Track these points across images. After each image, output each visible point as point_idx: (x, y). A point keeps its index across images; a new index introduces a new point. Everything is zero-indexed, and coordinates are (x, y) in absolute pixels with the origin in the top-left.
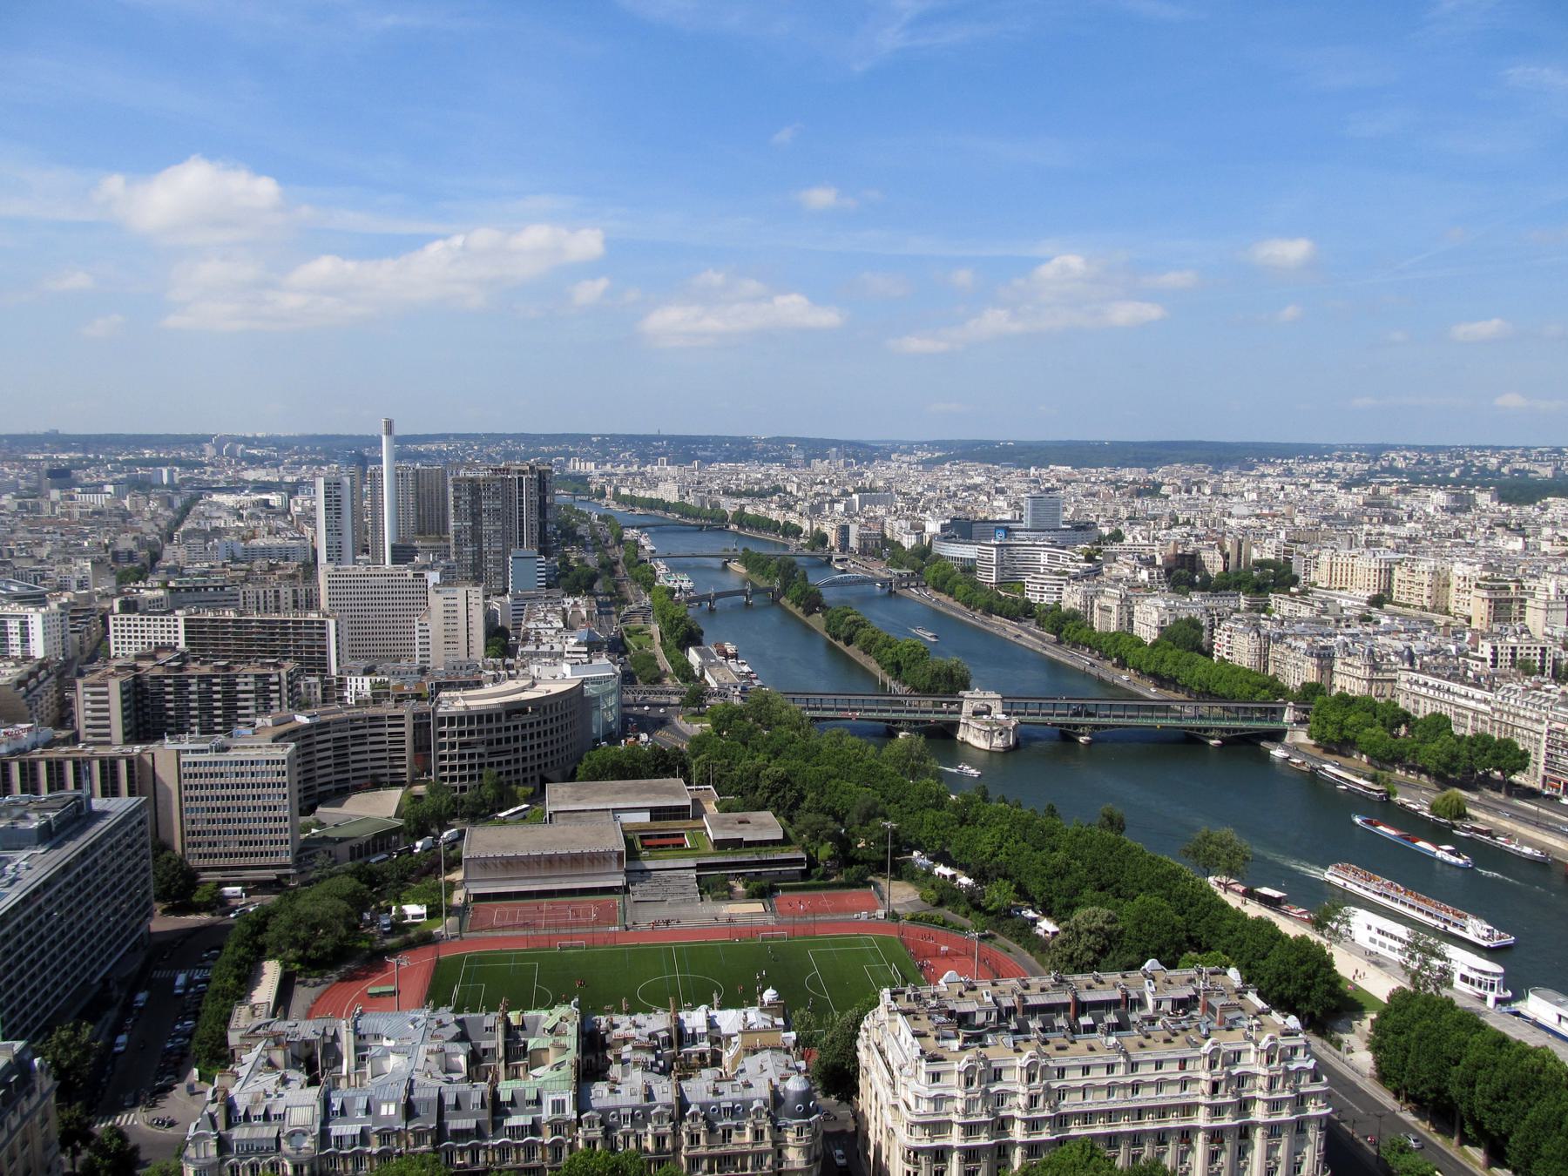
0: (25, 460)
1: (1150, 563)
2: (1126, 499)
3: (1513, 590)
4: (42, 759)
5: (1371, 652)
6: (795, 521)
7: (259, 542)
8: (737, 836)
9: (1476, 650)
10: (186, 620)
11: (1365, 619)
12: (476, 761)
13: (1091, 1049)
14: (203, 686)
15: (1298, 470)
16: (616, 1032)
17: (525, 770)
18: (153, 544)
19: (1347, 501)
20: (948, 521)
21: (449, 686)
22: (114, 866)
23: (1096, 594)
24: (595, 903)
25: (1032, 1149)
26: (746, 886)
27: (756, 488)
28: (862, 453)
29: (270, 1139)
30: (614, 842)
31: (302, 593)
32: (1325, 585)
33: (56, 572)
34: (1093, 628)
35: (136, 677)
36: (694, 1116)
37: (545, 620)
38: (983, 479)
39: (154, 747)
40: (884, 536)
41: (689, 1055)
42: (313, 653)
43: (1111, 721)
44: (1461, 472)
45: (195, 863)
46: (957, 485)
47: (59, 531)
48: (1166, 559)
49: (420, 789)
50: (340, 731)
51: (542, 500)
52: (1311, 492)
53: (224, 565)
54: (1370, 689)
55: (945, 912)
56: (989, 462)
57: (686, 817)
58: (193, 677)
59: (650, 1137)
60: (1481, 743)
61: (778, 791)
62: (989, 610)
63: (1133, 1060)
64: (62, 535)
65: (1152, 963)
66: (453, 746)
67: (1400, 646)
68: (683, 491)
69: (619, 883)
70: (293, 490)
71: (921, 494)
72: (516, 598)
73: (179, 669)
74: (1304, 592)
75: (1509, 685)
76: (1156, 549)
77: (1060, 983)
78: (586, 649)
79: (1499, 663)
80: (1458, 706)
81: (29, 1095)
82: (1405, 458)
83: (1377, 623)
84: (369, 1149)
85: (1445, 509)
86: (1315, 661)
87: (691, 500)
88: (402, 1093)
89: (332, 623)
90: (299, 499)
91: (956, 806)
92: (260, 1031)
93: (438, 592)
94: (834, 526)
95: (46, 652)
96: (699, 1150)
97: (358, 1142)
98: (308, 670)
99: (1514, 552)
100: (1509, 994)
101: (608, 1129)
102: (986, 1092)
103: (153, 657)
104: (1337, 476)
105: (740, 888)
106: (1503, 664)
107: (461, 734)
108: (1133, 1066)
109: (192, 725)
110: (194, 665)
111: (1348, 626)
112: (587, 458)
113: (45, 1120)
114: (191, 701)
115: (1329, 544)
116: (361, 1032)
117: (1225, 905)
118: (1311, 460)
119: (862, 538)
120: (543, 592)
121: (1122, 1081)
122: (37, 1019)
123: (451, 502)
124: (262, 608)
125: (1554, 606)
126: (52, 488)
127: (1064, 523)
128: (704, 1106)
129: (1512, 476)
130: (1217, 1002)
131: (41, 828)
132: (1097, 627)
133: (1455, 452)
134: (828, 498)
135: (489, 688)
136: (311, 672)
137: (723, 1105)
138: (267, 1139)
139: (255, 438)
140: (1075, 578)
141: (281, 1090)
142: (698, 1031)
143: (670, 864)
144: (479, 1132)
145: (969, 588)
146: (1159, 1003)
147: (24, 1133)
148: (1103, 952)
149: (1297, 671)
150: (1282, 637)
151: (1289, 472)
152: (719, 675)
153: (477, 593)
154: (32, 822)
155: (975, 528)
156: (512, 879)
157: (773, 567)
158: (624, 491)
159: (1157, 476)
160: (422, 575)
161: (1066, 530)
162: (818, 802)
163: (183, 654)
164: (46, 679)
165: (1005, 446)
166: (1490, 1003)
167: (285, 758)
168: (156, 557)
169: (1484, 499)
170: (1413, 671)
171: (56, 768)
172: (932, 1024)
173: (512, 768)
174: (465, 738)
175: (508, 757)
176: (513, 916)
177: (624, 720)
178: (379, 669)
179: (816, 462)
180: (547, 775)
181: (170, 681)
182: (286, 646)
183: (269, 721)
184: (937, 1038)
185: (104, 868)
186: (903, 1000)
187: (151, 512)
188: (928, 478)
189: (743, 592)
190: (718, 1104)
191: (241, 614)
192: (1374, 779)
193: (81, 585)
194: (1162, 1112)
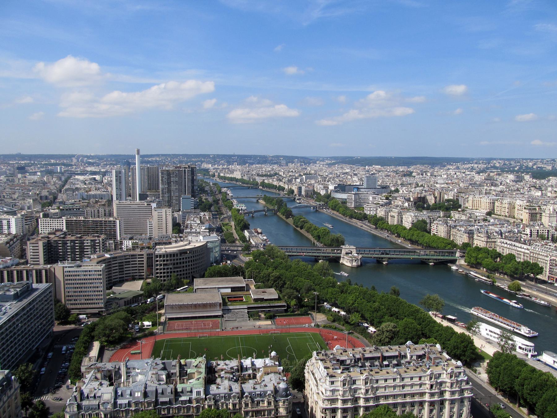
0: (9, 164)
1: (408, 200)
2: (400, 177)
3: (537, 210)
4: (15, 270)
5: (487, 232)
6: (282, 185)
7: (92, 193)
8: (262, 297)
9: (524, 231)
10: (66, 220)
11: (485, 220)
12: (169, 270)
13: (388, 373)
14: (72, 244)
15: (461, 167)
16: (219, 367)
17: (186, 274)
18: (54, 193)
19: (478, 178)
20: (337, 185)
21: (159, 244)
22: (41, 308)
23: (389, 211)
24: (211, 321)
25: (367, 408)
26: (265, 315)
27: (269, 173)
28: (306, 161)
29: (96, 405)
30: (218, 299)
31: (107, 211)
32: (471, 208)
33: (20, 203)
34: (388, 223)
35: (48, 241)
36: (247, 397)
37: (194, 221)
38: (349, 170)
39: (55, 265)
40: (314, 190)
41: (245, 375)
42: (111, 232)
43: (395, 256)
44: (519, 168)
45: (69, 307)
46: (340, 173)
47: (21, 189)
48: (414, 199)
49: (149, 281)
50: (121, 260)
51: (193, 178)
52: (466, 175)
53: (80, 201)
54: (487, 245)
56: (351, 164)
57: (244, 290)
58: (68, 241)
59: (231, 404)
60: (526, 264)
61: (276, 281)
62: (351, 217)
63: (403, 377)
64: (22, 190)
65: (409, 342)
66: (161, 265)
67: (497, 230)
68: (243, 174)
69: (220, 314)
71: (327, 176)
72: (183, 213)
73: (64, 238)
74: (463, 211)
75: (536, 244)
76: (411, 195)
77: (377, 349)
78: (208, 231)
79: (533, 236)
80: (518, 251)
81: (10, 389)
82: (499, 163)
83: (489, 221)
84: (131, 409)
85: (513, 181)
86: (467, 235)
87: (245, 178)
88: (143, 389)
89: (118, 221)
90: (106, 177)
91: (340, 287)
92: (93, 367)
93: (155, 210)
94: (296, 187)
95: (16, 232)
96: (248, 409)
97: (127, 406)
98: (109, 238)
99: (538, 196)
100: (536, 353)
101: (216, 401)
102: (350, 388)
103: (54, 234)
104: (475, 169)
105: (263, 316)
106: (534, 236)
107: (164, 261)
108: (403, 379)
109: (68, 258)
110: (69, 236)
111: (479, 223)
112: (208, 163)
113: (16, 398)
114: (68, 249)
115: (472, 193)
116: (128, 367)
117: (435, 322)
118: (466, 164)
119: (306, 191)
120: (193, 211)
121: (399, 384)
122: (13, 362)
123: (160, 179)
124: (93, 216)
125: (552, 215)
126: (19, 173)
127: (378, 186)
128: (250, 393)
129: (537, 169)
130: (432, 356)
131: (14, 294)
132: (390, 223)
133: (517, 161)
134: (294, 177)
135: (174, 245)
136: (111, 239)
137: (257, 393)
138: (95, 405)
139: (91, 156)
140: (382, 205)
141: (100, 387)
142: (248, 366)
143: (238, 307)
144: (170, 402)
146: (412, 357)
147: (9, 403)
148: (392, 338)
149: (461, 239)
150: (455, 226)
151: (458, 168)
152: (255, 240)
153: (169, 211)
154: (11, 292)
155: (347, 188)
156: (182, 312)
157: (274, 201)
158: (222, 175)
159: (411, 169)
160: (150, 204)
161: (379, 188)
162: (291, 285)
164: (16, 241)
165: (357, 159)
166: (529, 356)
167: (101, 269)
168: (55, 198)
169: (527, 177)
170: (502, 238)
171: (20, 273)
172: (331, 364)
173: (182, 273)
174: (165, 262)
175: (180, 269)
176: (182, 326)
177: (222, 256)
178: (135, 238)
179: (290, 164)
180: (194, 276)
181: (60, 242)
182: (102, 230)
183: (95, 256)
184: (333, 369)
185: (37, 309)
186: (321, 356)
187: (54, 182)
188: (330, 170)
189: (264, 211)
190: (255, 392)
191: (86, 218)
192: (488, 277)
193: (29, 208)
194: (413, 395)
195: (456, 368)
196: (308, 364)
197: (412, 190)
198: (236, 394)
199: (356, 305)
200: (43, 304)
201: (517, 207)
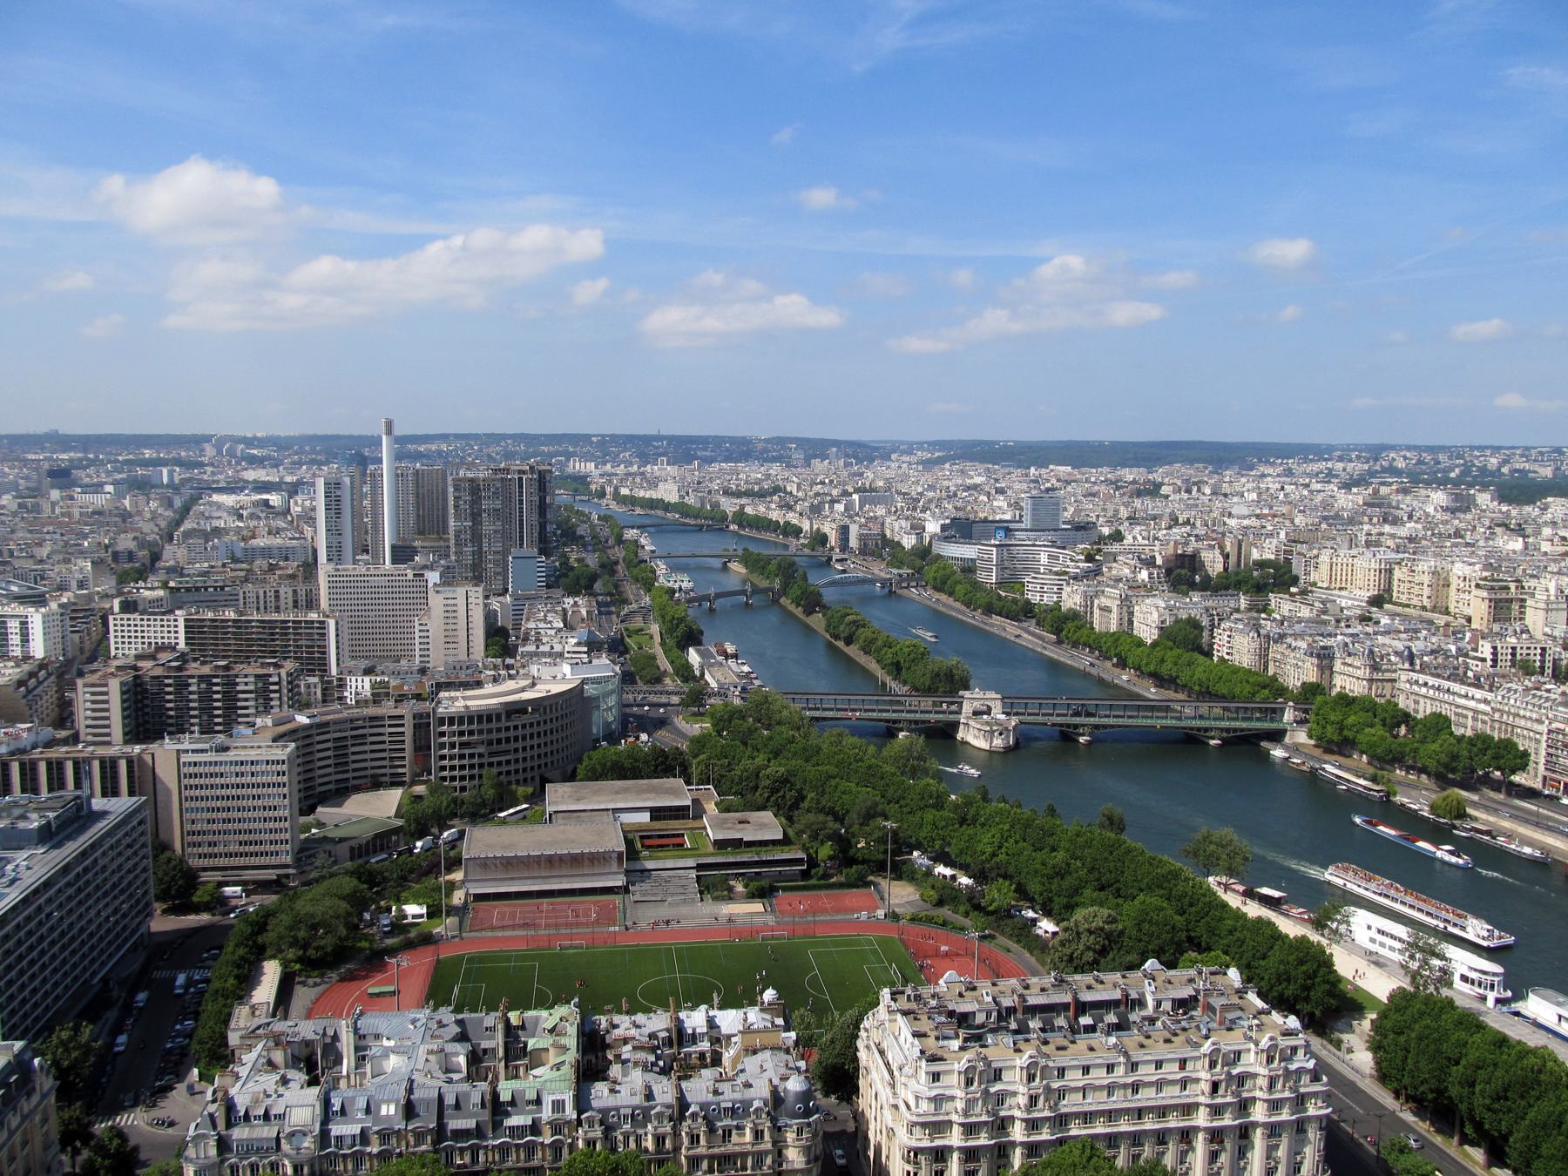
0: (25, 460)
1: (1150, 563)
2: (1126, 499)
3: (1513, 590)
4: (42, 759)
5: (1371, 652)
6: (795, 521)
7: (259, 542)
8: (737, 836)
9: (1476, 650)
10: (186, 620)
11: (1365, 619)
12: (476, 761)
13: (1091, 1049)
14: (203, 686)
15: (1298, 470)
16: (616, 1032)
17: (525, 770)
18: (153, 544)
19: (1347, 501)
20: (948, 521)
21: (449, 686)
22: (114, 866)
23: (1096, 594)
24: (595, 903)
25: (1032, 1149)
26: (746, 886)
27: (756, 488)
28: (862, 453)
29: (270, 1139)
30: (614, 842)
31: (302, 593)
32: (1325, 585)
33: (56, 572)
34: (1093, 628)
35: (136, 677)
36: (694, 1116)
37: (545, 620)
38: (983, 479)
39: (154, 747)
40: (884, 536)
41: (689, 1055)
42: (313, 653)
43: (1111, 721)
44: (1461, 472)
45: (195, 863)
46: (957, 485)
47: (59, 531)
48: (1166, 559)
49: (420, 789)
50: (340, 731)
51: (542, 500)
52: (1311, 492)
53: (224, 565)
54: (1370, 689)
55: (945, 912)
56: (989, 462)
57: (686, 817)
58: (193, 677)
59: (650, 1137)
60: (1481, 743)
61: (778, 791)
62: (989, 610)
63: (1133, 1060)
64: (62, 535)
65: (1152, 963)
66: (453, 746)
67: (1400, 646)
68: (683, 491)
69: (619, 883)
70: (293, 490)
71: (921, 494)
72: (516, 598)
73: (179, 669)
74: (1304, 592)
75: (1509, 685)
76: (1156, 549)
77: (1060, 983)
78: (586, 649)
79: (1499, 663)
80: (1458, 706)
81: (29, 1095)
82: (1405, 458)
83: (1377, 623)
84: (369, 1149)
85: (1445, 509)
86: (1315, 661)
87: (691, 500)
88: (402, 1093)
89: (332, 623)
90: (299, 499)
91: (956, 806)
92: (260, 1031)
93: (438, 592)
94: (834, 526)
95: (46, 652)
96: (699, 1150)
97: (358, 1142)
98: (308, 670)
99: (1514, 552)
100: (1509, 994)
101: (608, 1129)
102: (986, 1092)
103: (153, 657)
104: (1337, 476)
105: (740, 888)
107: (461, 734)
108: (1133, 1066)
109: (192, 725)
111: (1348, 626)
112: (587, 458)
113: (45, 1120)
114: (191, 701)
115: (1329, 544)
116: (361, 1032)
117: (1225, 905)
118: (1311, 460)
119: (862, 538)
120: (543, 592)
121: (1122, 1081)
122: (37, 1019)
123: (451, 502)
124: (262, 608)
125: (1554, 606)
126: (52, 488)
127: (1064, 523)
128: (704, 1106)
129: (1512, 476)
130: (1217, 1002)
131: (41, 828)
132: (1097, 627)
133: (1455, 452)
134: (828, 498)
135: (489, 688)
136: (311, 672)
137: (723, 1105)
138: (267, 1139)
139: (255, 438)
140: (1075, 578)
141: (281, 1090)
142: (698, 1031)
143: (670, 864)
144: (479, 1132)
145: (969, 588)
146: (1159, 1003)
147: (24, 1133)
148: (1103, 952)
149: (1297, 671)
150: (1282, 637)
151: (1289, 472)
152: (719, 675)
154: (32, 822)
155: (975, 528)
156: (512, 879)
157: (773, 567)
158: (624, 491)
159: (1157, 476)
160: (422, 575)
161: (1066, 530)
162: (818, 802)
163: (183, 654)
164: (46, 679)
165: (1005, 446)
166: (1490, 1003)
167: (285, 758)
168: (156, 557)
169: (1484, 499)
170: (1413, 671)
171: (56, 768)
172: (932, 1024)
173: (512, 768)
174: (465, 738)
175: (508, 757)
176: (513, 916)
177: (624, 720)
178: (379, 669)
179: (816, 462)
180: (547, 775)
181: (170, 681)
182: (286, 646)
183: (269, 721)
184: (937, 1038)
185: (104, 868)
186: (903, 1000)
188: (928, 478)
189: (743, 592)
190: (718, 1104)
191: (241, 614)
192: (1374, 779)
193: (81, 585)
194: (1162, 1112)
195: (1284, 1035)
196: (866, 1024)
197: (1161, 534)
198: (664, 1110)
199: (1002, 857)
200: (120, 854)
201: (1455, 583)
